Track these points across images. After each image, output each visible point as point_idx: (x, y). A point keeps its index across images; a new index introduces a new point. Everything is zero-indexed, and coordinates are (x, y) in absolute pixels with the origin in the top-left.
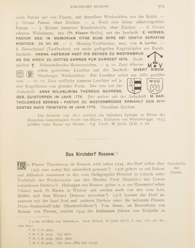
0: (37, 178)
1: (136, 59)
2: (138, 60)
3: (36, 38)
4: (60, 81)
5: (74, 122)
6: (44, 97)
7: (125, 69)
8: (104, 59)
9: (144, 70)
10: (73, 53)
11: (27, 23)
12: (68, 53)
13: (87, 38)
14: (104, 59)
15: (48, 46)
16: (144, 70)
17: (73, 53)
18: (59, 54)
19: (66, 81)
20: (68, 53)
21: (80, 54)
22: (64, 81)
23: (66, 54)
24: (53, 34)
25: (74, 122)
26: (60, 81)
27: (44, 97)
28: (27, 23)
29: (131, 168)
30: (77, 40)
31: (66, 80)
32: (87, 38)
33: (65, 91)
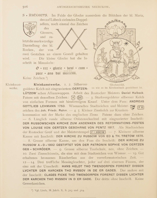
0: (104, 172)
1: (128, 128)
2: (130, 128)
3: (99, 123)
4: (47, 162)
5: (63, 160)
6: (92, 175)
7: (51, 131)
8: (80, 128)
9: (58, 128)
10: (133, 92)
11: (37, 141)
12: (132, 101)
13: (87, 179)
14: (80, 128)
15: (80, 138)
16: (58, 128)
17: (133, 92)
18: (134, 123)
19: (52, 162)
20: (132, 101)
21: (27, 106)
22: (51, 162)
23: (50, 106)
24: (69, 141)
25: (63, 160)
26: (47, 162)
27: (92, 175)
28: (37, 141)
29: (49, 153)
30: (45, 163)
31: (52, 162)
32: (87, 179)
33: (76, 166)
